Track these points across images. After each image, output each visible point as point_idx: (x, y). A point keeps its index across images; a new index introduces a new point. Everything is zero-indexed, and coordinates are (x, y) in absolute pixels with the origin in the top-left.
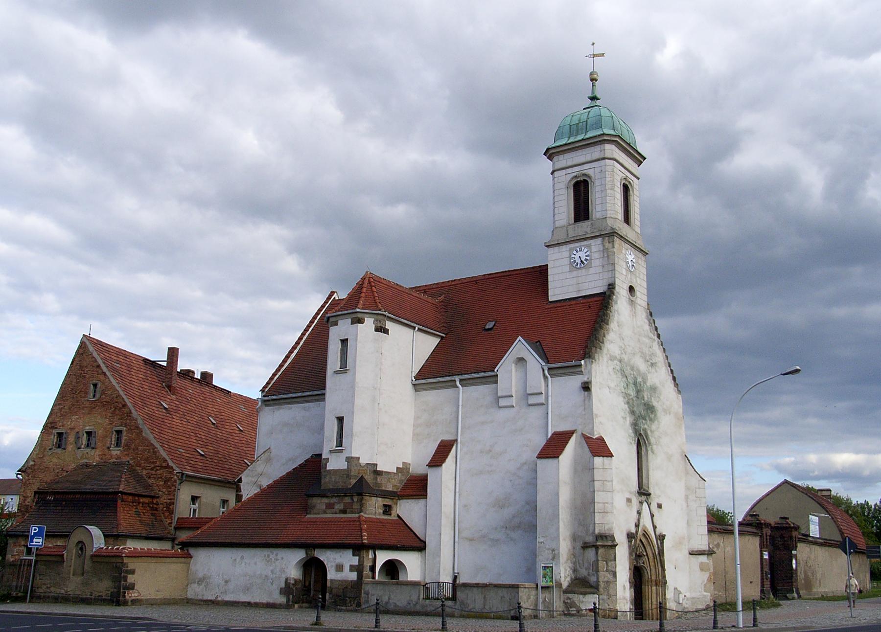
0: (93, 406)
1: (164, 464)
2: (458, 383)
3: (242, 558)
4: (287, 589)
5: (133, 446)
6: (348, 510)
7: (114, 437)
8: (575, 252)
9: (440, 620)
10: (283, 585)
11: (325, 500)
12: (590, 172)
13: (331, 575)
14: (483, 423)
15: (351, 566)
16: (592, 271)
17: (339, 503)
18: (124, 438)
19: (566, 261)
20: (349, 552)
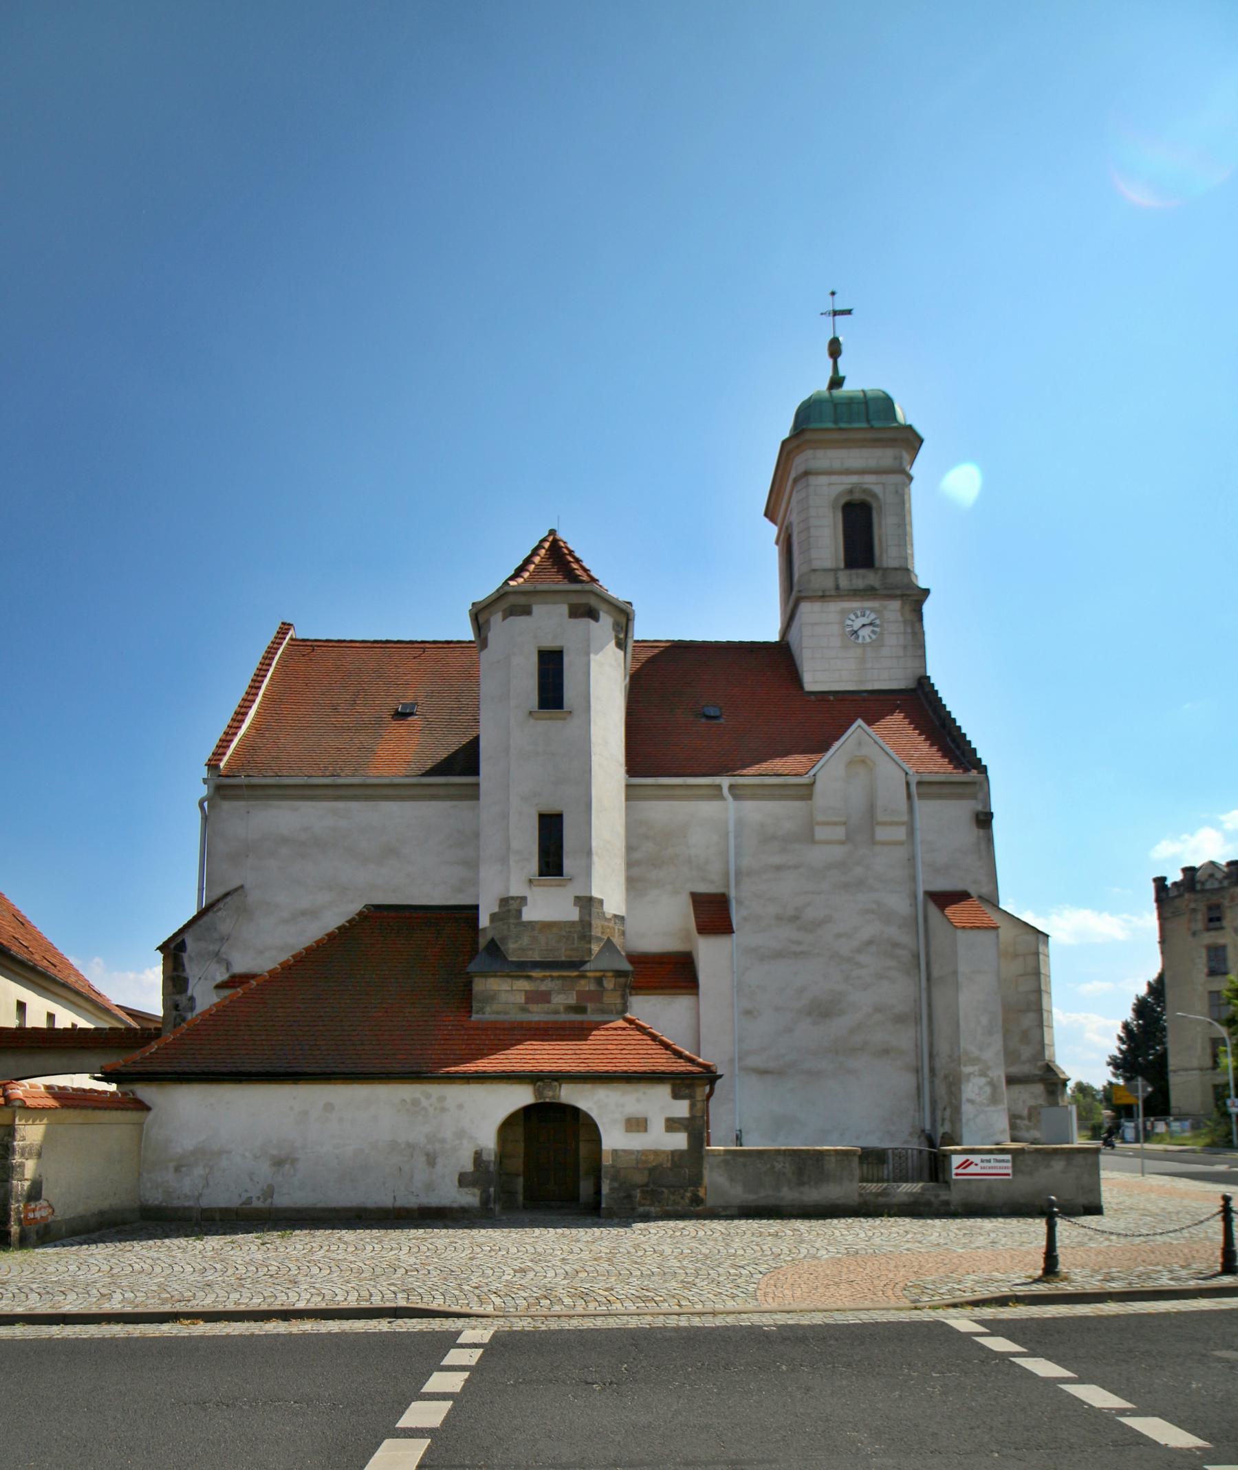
2: (725, 791)
4: (480, 1174)
6: (590, 1006)
8: (853, 617)
9: (1040, 1225)
10: (469, 1167)
11: (523, 985)
12: (877, 489)
13: (614, 1139)
14: (779, 868)
17: (562, 991)
19: (835, 629)
20: (664, 1091)
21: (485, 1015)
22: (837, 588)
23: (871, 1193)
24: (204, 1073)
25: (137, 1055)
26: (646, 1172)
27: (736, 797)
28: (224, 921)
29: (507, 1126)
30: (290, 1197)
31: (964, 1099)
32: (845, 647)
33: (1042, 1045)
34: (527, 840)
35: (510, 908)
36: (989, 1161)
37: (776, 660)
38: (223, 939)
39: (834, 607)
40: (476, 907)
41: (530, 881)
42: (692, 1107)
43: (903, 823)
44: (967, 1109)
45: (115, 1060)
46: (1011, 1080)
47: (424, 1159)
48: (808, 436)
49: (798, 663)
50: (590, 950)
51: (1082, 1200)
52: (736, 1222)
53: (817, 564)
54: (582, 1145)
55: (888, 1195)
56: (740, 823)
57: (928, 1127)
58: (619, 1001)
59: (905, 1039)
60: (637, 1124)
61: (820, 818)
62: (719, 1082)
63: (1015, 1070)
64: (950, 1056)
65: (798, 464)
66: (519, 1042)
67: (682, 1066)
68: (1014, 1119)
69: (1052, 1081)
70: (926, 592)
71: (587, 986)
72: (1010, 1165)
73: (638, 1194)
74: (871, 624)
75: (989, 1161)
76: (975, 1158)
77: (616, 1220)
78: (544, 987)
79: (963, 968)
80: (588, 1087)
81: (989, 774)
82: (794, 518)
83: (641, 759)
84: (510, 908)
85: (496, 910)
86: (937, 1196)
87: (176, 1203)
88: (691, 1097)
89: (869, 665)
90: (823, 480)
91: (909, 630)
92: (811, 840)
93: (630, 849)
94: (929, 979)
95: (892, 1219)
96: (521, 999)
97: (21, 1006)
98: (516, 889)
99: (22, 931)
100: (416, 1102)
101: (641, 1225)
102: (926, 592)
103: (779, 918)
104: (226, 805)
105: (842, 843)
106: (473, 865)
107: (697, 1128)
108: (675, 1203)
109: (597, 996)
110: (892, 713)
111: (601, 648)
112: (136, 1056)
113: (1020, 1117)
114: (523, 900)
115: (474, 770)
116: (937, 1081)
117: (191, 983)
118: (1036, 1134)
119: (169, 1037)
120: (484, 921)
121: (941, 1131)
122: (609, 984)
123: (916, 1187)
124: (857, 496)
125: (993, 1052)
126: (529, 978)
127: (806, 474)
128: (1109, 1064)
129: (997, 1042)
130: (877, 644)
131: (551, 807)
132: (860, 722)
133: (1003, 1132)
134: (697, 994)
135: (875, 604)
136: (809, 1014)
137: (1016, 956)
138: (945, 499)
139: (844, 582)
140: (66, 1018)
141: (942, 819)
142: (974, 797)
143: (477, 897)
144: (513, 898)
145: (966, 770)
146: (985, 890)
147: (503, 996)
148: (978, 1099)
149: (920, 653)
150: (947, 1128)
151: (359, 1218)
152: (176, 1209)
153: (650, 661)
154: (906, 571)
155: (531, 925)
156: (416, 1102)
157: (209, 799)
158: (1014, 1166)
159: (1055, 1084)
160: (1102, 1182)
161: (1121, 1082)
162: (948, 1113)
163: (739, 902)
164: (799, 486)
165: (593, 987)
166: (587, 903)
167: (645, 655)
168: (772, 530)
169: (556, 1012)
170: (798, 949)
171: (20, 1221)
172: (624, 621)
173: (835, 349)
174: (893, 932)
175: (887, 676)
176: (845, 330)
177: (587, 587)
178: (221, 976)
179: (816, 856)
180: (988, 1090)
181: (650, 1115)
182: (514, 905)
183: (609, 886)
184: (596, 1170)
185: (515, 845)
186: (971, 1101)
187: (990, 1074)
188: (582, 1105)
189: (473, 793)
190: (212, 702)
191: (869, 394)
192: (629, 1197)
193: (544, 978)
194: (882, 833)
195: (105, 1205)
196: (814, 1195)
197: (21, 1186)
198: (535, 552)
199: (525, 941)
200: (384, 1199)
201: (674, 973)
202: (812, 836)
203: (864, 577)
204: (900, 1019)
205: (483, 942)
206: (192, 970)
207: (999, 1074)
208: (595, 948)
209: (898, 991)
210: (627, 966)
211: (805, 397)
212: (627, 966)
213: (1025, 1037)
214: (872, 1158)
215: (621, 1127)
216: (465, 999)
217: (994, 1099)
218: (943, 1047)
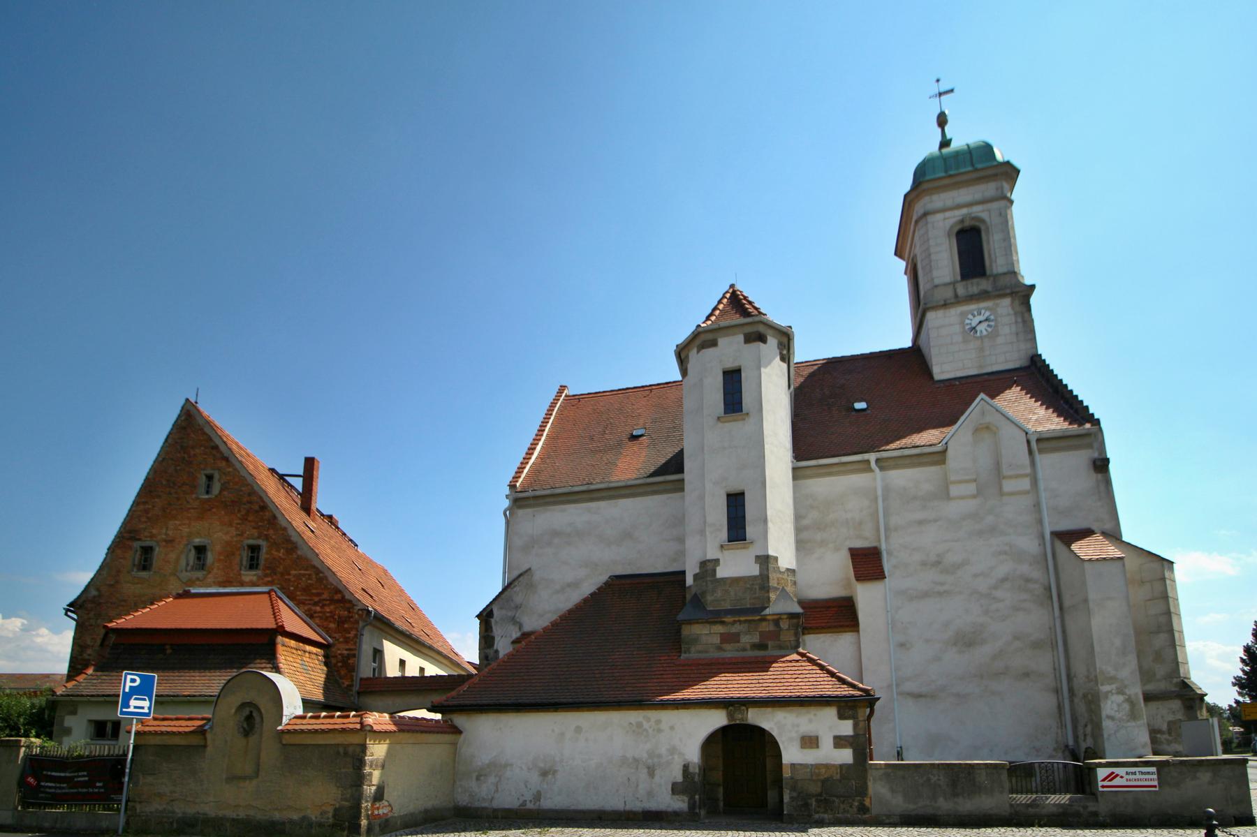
0: (205, 509)
1: (338, 597)
3: (578, 730)
4: (686, 785)
5: (281, 569)
6: (770, 644)
7: (245, 555)
10: (679, 778)
11: (719, 629)
12: (984, 216)
13: (792, 754)
14: (921, 523)
15: (836, 738)
16: (1000, 340)
18: (263, 555)
19: (957, 328)
20: (831, 712)
21: (693, 654)
22: (956, 296)
23: (1021, 804)
24: (496, 705)
25: (454, 693)
26: (820, 784)
27: (882, 469)
28: (518, 596)
29: (710, 743)
30: (553, 801)
31: (1104, 714)
32: (965, 341)
33: (1176, 663)
34: (718, 514)
35: (708, 568)
36: (1134, 773)
37: (910, 361)
38: (517, 607)
39: (955, 312)
40: (684, 572)
41: (722, 546)
42: (855, 726)
43: (1026, 475)
44: (1107, 724)
45: (437, 698)
46: (1148, 698)
47: (646, 771)
48: (925, 186)
49: (928, 359)
50: (769, 598)
51: (1232, 811)
52: (899, 829)
53: (937, 282)
54: (768, 760)
55: (1038, 806)
56: (887, 489)
57: (1071, 742)
58: (793, 638)
59: (1043, 663)
60: (810, 742)
61: (953, 478)
62: (878, 703)
63: (1150, 687)
64: (1087, 677)
65: (919, 209)
66: (716, 674)
67: (845, 691)
68: (1154, 733)
69: (1190, 698)
70: (1032, 287)
71: (767, 627)
72: (1155, 777)
73: (813, 802)
74: (987, 320)
75: (1134, 773)
76: (1120, 771)
77: (796, 826)
78: (735, 629)
79: (1092, 596)
80: (769, 710)
81: (1102, 425)
82: (918, 250)
83: (806, 446)
84: (708, 568)
85: (697, 571)
86: (1085, 807)
87: (477, 804)
88: (854, 717)
89: (987, 353)
90: (939, 216)
91: (1020, 320)
92: (948, 497)
93: (798, 517)
94: (1061, 608)
95: (1043, 829)
96: (717, 640)
97: (402, 663)
98: (711, 554)
99: (412, 613)
100: (639, 725)
101: (816, 830)
102: (1032, 287)
103: (924, 564)
104: (521, 512)
105: (974, 497)
106: (681, 540)
107: (861, 744)
108: (845, 811)
109: (775, 635)
110: (1010, 388)
111: (770, 362)
112: (458, 696)
113: (1160, 731)
114: (717, 561)
115: (680, 469)
116: (1076, 700)
117: (497, 639)
118: (1179, 748)
119: (476, 680)
120: (689, 581)
121: (1083, 746)
122: (784, 625)
123: (1064, 798)
124: (967, 224)
125: (1128, 671)
126: (723, 623)
127: (925, 214)
128: (1234, 684)
129: (1132, 662)
130: (993, 335)
131: (735, 487)
132: (982, 395)
133: (1144, 746)
134: (858, 631)
135: (989, 304)
136: (955, 644)
137: (1143, 582)
138: (1037, 238)
139: (961, 290)
140: (432, 670)
141: (1064, 471)
142: (1090, 446)
143: (684, 563)
144: (709, 561)
145: (1081, 424)
146: (1108, 526)
147: (705, 637)
148: (1118, 715)
149: (1030, 336)
150: (1089, 742)
151: (600, 818)
152: (477, 809)
153: (812, 375)
154: (1014, 273)
155: (723, 580)
156: (639, 725)
157: (510, 509)
158: (1159, 779)
159: (1193, 700)
160: (1252, 792)
161: (1248, 700)
162: (1089, 729)
163: (889, 553)
164: (921, 224)
165: (772, 628)
166: (765, 561)
167: (806, 372)
168: (901, 264)
169: (744, 650)
170: (941, 589)
171: (368, 817)
172: (785, 340)
173: (942, 120)
174: (1025, 569)
175: (1005, 358)
176: (948, 104)
177: (756, 319)
178: (516, 634)
179: (953, 509)
180: (1126, 706)
181: (820, 734)
182: (710, 566)
183: (781, 544)
184: (779, 782)
185: (710, 519)
186: (1111, 718)
187: (1127, 691)
188: (766, 725)
189: (679, 487)
190: (511, 439)
191: (972, 146)
192: (806, 805)
193: (735, 622)
194: (1008, 486)
195: (429, 804)
196: (967, 805)
197: (369, 790)
198: (720, 302)
199: (719, 594)
200: (614, 803)
201: (838, 615)
202: (948, 494)
203: (978, 284)
204: (1036, 645)
205: (688, 597)
206: (497, 631)
207: (1136, 691)
208: (773, 596)
209: (1035, 620)
210: (798, 610)
211: (920, 160)
212: (798, 610)
213: (1158, 657)
214: (1020, 773)
215: (797, 744)
216: (676, 642)
217: (1133, 715)
218: (1080, 669)
